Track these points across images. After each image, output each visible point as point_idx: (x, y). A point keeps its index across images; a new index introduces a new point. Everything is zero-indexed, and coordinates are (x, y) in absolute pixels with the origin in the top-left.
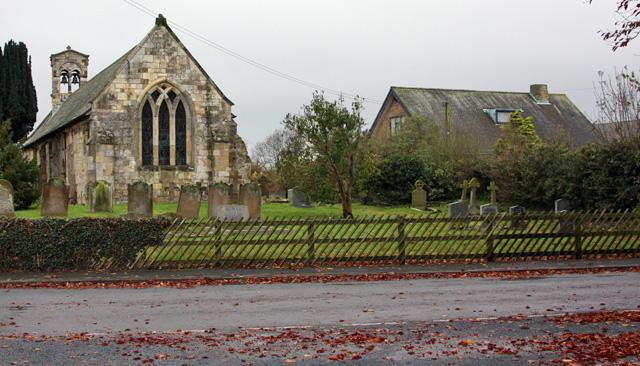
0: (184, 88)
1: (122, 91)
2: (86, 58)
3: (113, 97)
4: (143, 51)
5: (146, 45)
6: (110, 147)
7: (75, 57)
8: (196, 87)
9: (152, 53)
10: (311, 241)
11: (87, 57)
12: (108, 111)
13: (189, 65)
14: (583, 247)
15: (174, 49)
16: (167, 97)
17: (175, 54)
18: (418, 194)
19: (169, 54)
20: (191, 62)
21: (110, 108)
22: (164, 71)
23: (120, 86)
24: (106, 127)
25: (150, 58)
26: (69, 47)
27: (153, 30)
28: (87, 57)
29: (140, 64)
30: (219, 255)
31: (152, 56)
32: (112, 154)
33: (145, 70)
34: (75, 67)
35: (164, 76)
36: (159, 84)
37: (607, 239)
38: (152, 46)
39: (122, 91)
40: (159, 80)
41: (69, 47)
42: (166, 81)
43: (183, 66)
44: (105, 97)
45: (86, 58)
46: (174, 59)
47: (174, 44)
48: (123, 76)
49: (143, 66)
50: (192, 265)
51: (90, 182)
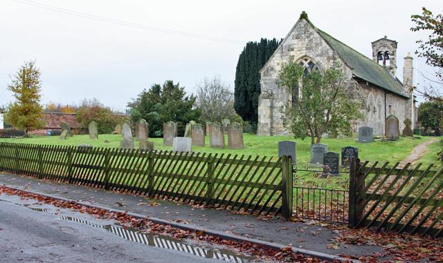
0: (318, 59)
1: (278, 64)
2: (395, 44)
3: (272, 69)
4: (291, 37)
5: (293, 33)
6: (268, 100)
7: (386, 43)
8: (326, 58)
9: (297, 38)
10: (17, 159)
11: (372, 43)
12: (269, 78)
13: (321, 43)
14: (155, 188)
15: (311, 34)
16: (308, 66)
17: (312, 37)
18: (93, 128)
19: (308, 37)
20: (323, 41)
21: (271, 75)
22: (304, 49)
23: (277, 61)
24: (268, 88)
25: (295, 41)
26: (386, 37)
27: (297, 23)
28: (372, 43)
29: (290, 46)
30: (210, 195)
31: (296, 40)
32: (269, 104)
33: (293, 50)
34: (386, 49)
35: (304, 52)
36: (302, 58)
37: (188, 183)
38: (297, 33)
39: (278, 64)
40: (301, 56)
41: (386, 37)
42: (306, 56)
43: (317, 44)
44: (268, 69)
45: (395, 44)
46: (311, 40)
47: (311, 30)
48: (279, 55)
49: (292, 47)
50: (59, 177)
51: (369, 135)
